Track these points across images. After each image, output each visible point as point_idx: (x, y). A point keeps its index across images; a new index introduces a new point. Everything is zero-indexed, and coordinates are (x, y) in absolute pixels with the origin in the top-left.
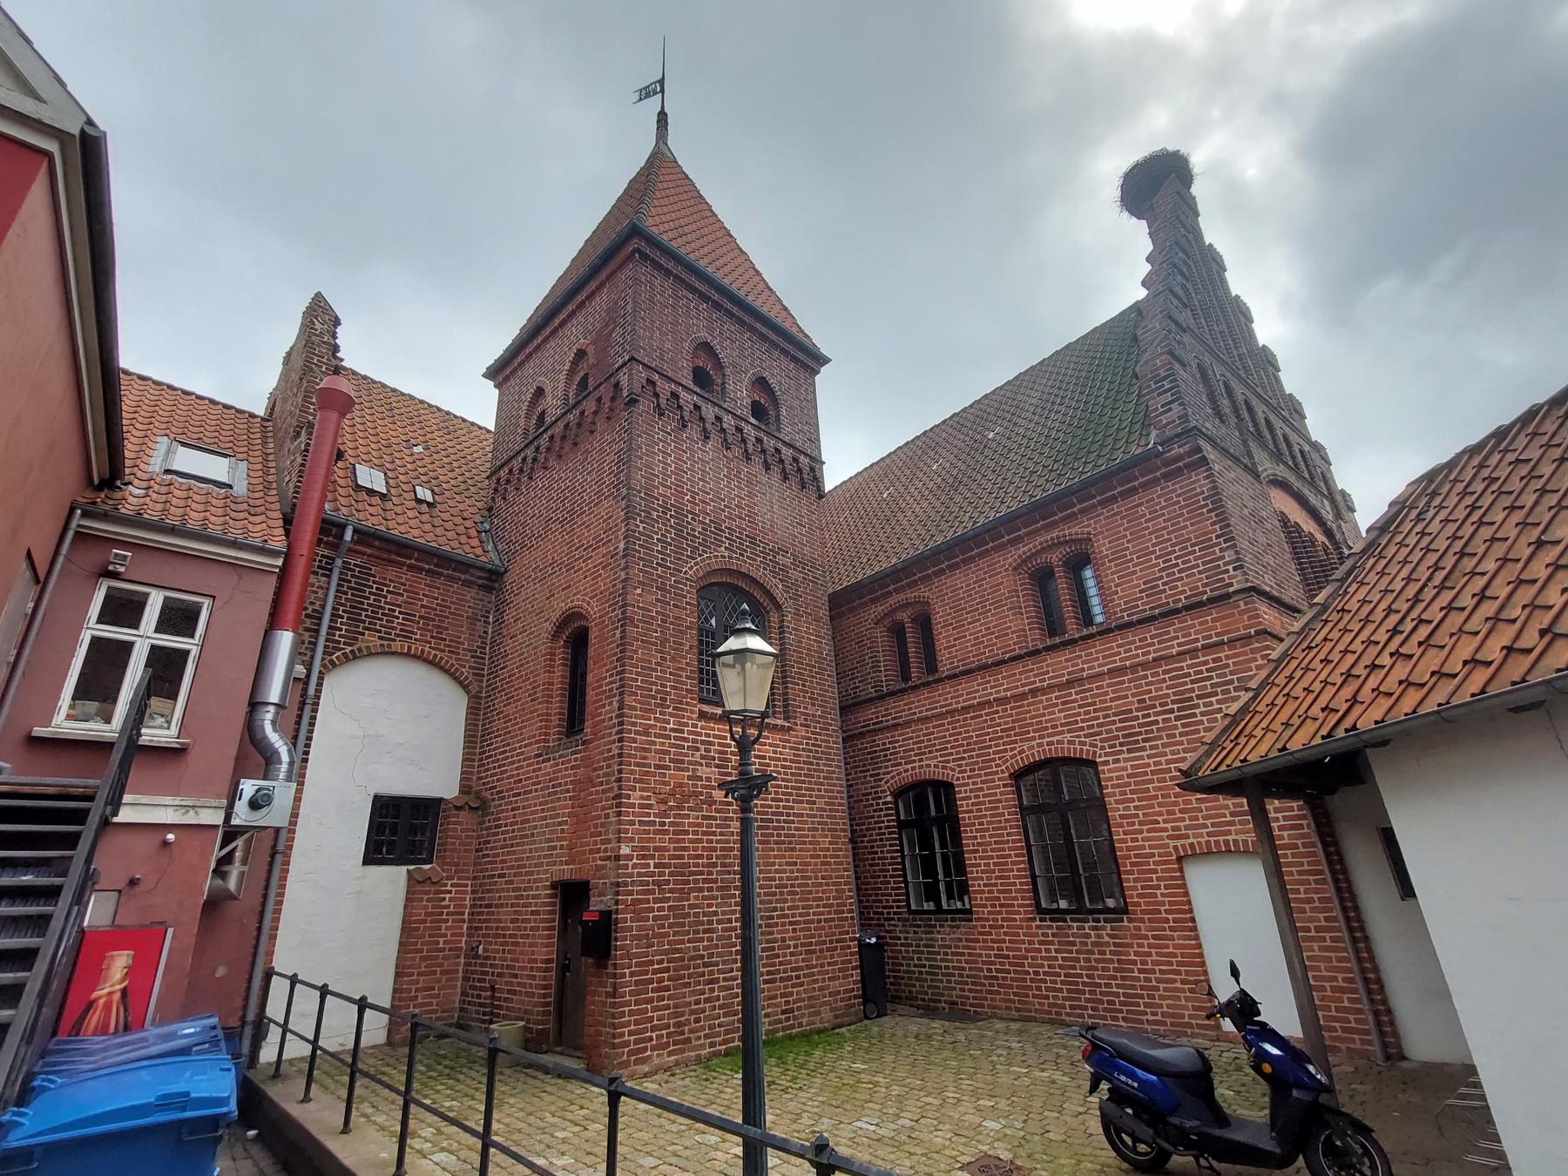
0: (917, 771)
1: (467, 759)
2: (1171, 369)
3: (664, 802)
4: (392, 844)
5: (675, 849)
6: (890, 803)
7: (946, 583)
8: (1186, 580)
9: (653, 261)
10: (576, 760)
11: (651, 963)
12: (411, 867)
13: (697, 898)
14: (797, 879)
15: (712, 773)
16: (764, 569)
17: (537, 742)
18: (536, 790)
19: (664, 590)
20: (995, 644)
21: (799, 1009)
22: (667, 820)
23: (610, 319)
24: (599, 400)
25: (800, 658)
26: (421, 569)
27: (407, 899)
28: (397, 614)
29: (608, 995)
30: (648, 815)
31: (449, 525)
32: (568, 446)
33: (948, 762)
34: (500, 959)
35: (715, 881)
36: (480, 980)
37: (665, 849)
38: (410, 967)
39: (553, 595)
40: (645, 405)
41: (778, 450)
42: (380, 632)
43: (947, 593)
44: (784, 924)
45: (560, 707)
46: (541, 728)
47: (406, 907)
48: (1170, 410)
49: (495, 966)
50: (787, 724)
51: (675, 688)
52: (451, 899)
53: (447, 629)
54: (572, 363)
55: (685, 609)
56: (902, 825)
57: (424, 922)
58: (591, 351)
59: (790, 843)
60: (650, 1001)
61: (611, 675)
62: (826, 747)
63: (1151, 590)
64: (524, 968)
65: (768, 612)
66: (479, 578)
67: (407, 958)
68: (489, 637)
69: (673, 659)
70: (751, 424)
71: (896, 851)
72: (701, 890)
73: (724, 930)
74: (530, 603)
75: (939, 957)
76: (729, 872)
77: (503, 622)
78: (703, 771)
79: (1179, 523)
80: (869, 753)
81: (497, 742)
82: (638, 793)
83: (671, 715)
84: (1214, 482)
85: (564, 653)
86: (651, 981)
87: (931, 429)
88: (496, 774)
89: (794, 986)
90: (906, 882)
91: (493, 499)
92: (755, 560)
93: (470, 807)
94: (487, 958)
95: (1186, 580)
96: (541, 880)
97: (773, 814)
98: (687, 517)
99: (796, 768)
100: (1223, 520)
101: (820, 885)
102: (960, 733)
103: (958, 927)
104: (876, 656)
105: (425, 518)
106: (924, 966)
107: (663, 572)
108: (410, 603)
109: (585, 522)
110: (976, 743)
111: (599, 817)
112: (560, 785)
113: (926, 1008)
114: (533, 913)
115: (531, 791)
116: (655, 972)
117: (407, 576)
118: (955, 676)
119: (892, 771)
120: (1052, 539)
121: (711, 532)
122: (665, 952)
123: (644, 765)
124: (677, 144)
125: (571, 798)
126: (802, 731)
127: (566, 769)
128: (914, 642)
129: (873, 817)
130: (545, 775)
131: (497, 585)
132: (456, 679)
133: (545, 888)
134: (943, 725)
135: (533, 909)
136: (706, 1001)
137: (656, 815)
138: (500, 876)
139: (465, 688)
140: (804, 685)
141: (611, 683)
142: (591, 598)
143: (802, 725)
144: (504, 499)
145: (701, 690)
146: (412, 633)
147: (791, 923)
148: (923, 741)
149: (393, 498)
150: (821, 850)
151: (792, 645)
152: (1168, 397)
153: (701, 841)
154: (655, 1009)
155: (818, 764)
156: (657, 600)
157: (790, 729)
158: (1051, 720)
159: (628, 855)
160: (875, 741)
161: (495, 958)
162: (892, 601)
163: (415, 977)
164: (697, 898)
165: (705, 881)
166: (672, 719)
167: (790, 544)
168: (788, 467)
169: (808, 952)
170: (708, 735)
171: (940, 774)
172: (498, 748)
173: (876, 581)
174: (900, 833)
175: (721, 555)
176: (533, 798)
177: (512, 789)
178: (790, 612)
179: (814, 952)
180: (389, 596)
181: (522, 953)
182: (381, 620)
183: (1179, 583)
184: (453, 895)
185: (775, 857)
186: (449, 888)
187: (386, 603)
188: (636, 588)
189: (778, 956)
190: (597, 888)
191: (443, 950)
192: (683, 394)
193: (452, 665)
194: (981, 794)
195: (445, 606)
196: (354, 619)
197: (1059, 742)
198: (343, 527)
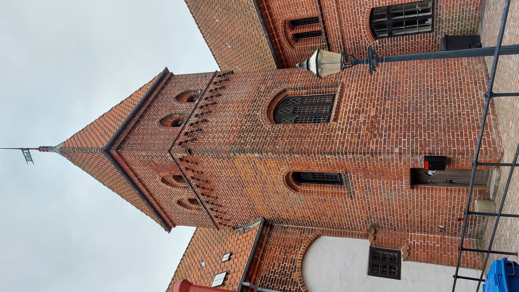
0: (365, 27)
1: (352, 236)
3: (375, 136)
4: (390, 268)
5: (397, 130)
6: (379, 41)
7: (276, 12)
9: (121, 143)
10: (354, 177)
11: (449, 139)
12: (402, 259)
13: (420, 121)
14: (413, 80)
15: (362, 116)
16: (267, 96)
17: (345, 199)
18: (368, 198)
19: (277, 137)
21: (475, 78)
22: (384, 134)
23: (148, 164)
24: (187, 169)
26: (263, 255)
27: (417, 261)
29: (463, 157)
30: (381, 142)
31: (241, 245)
32: (208, 186)
33: (361, 11)
34: (446, 216)
35: (413, 114)
36: (456, 227)
37: (397, 134)
38: (448, 258)
39: (277, 191)
40: (191, 146)
41: (211, 91)
42: (292, 272)
43: (281, 11)
44: (435, 85)
45: (329, 187)
46: (338, 196)
47: (421, 262)
49: (449, 218)
50: (340, 85)
52: (418, 241)
54: (167, 184)
55: (286, 128)
56: (391, 35)
57: (428, 253)
58: (163, 174)
59: (396, 83)
60: (467, 140)
61: (316, 159)
64: (450, 203)
65: (287, 95)
66: (267, 230)
67: (445, 260)
68: (294, 226)
69: (309, 133)
70: (199, 102)
71: (403, 38)
72: (417, 120)
73: (436, 110)
74: (280, 204)
75: (454, 16)
76: (409, 108)
77: (288, 218)
78: (361, 119)
80: (355, 52)
81: (344, 221)
82: (371, 146)
83: (335, 133)
85: (304, 186)
86: (458, 139)
87: (197, 24)
88: (359, 221)
89: (464, 81)
90: (418, 33)
91: (229, 226)
92: (263, 101)
93: (375, 233)
94: (445, 223)
96: (410, 194)
97: (382, 90)
98: (243, 128)
99: (361, 81)
101: (417, 70)
102: (348, 5)
103: (440, 6)
104: (309, 48)
105: (238, 255)
106: (459, 24)
109: (244, 175)
111: (381, 164)
112: (365, 185)
113: (478, 22)
114: (425, 199)
115: (368, 201)
116: (453, 137)
117: (266, 261)
118: (321, 7)
121: (250, 119)
122: (445, 133)
123: (358, 144)
124: (55, 142)
125: (372, 179)
126: (344, 79)
127: (358, 182)
128: (303, 29)
129: (386, 49)
130: (360, 194)
131: (270, 223)
133: (413, 192)
134: (343, 13)
135: (423, 198)
136: (468, 116)
137: (381, 138)
138: (407, 217)
139: (318, 237)
141: (319, 159)
142: (279, 170)
143: (341, 79)
144: (229, 220)
146: (292, 258)
147: (435, 82)
148: (351, 24)
149: (228, 269)
150: (400, 70)
151: (303, 84)
153: (394, 120)
154: (471, 137)
155: (360, 72)
156: (281, 139)
157: (342, 84)
159: (399, 150)
161: (446, 219)
162: (283, 39)
163: (454, 256)
164: (420, 121)
165: (413, 118)
166: (337, 133)
167: (255, 86)
168: (218, 87)
169: (449, 75)
170: (345, 118)
171: (367, 16)
172: (347, 219)
173: (273, 47)
174: (394, 36)
175: (261, 115)
176: (371, 200)
177: (367, 211)
179: (448, 73)
180: (275, 268)
181: (443, 204)
182: (286, 272)
184: (416, 241)
185: (403, 89)
186: (412, 242)
187: (278, 270)
188: (276, 148)
189: (449, 88)
190: (414, 164)
191: (441, 245)
192: (186, 130)
193: (307, 242)
196: (286, 282)
198: (243, 286)
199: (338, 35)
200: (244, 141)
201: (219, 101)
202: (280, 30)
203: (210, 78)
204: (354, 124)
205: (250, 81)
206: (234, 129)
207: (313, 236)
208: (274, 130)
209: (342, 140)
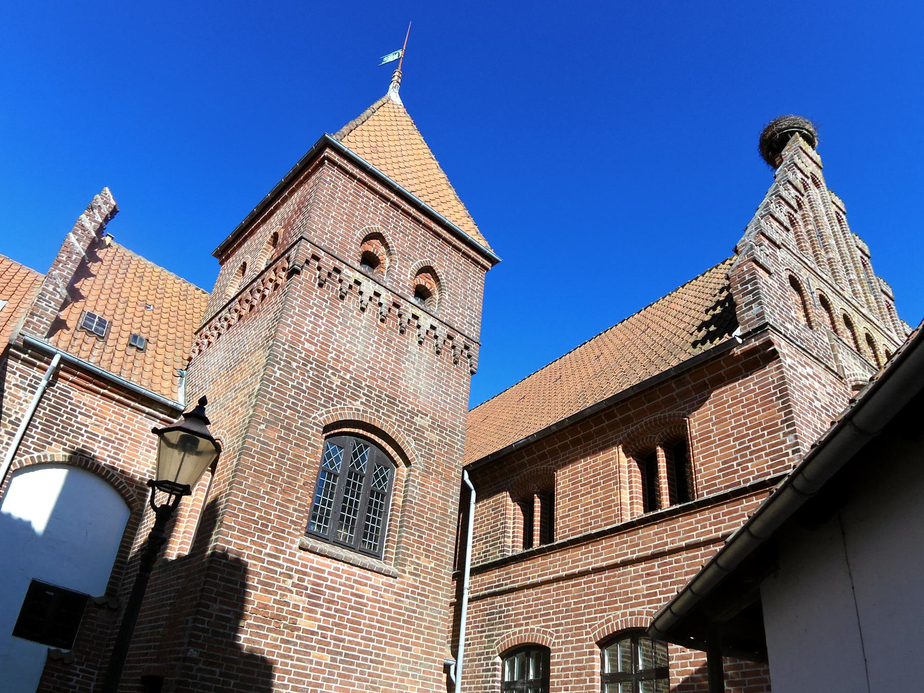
2: (754, 273)
8: (755, 462)
20: (600, 516)
25: (422, 511)
28: (83, 432)
40: (308, 276)
42: (65, 444)
48: (751, 308)
51: (280, 517)
53: (124, 452)
55: (307, 449)
62: (434, 599)
63: (727, 470)
69: (283, 491)
78: (293, 598)
79: (753, 409)
83: (269, 540)
84: (782, 372)
95: (755, 462)
100: (787, 408)
107: (292, 414)
108: (96, 425)
110: (573, 610)
119: (503, 633)
120: (655, 420)
123: (230, 581)
126: (409, 579)
132: (123, 496)
140: (420, 537)
143: (410, 573)
145: (309, 524)
151: (415, 498)
152: (750, 297)
156: (280, 437)
158: (635, 591)
160: (493, 603)
171: (539, 639)
178: (418, 469)
182: (68, 435)
183: (749, 465)
187: (75, 422)
188: (259, 424)
192: (346, 271)
194: (570, 660)
195: (126, 432)
197: (640, 613)
199: (518, 581)
200: (294, 367)
201: (408, 339)
202: (541, 465)
203: (464, 331)
204: (284, 581)
205: (445, 402)
206: (330, 355)
207: (132, 496)
208: (307, 426)
209: (247, 552)
